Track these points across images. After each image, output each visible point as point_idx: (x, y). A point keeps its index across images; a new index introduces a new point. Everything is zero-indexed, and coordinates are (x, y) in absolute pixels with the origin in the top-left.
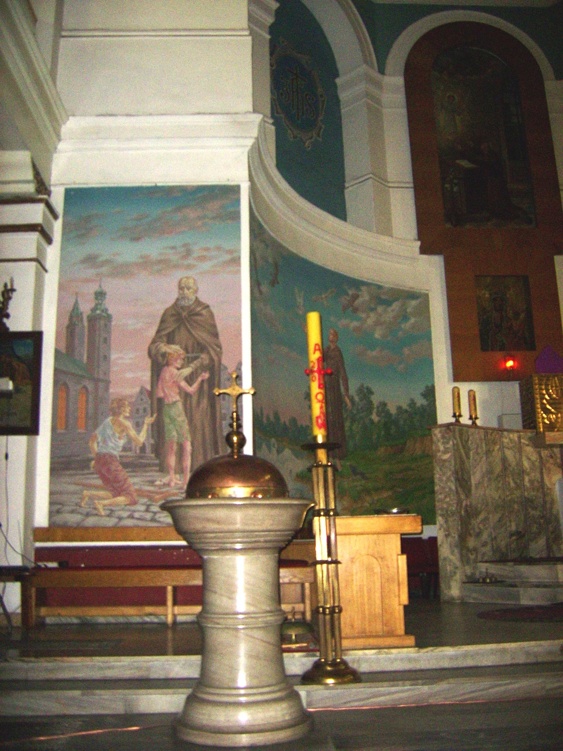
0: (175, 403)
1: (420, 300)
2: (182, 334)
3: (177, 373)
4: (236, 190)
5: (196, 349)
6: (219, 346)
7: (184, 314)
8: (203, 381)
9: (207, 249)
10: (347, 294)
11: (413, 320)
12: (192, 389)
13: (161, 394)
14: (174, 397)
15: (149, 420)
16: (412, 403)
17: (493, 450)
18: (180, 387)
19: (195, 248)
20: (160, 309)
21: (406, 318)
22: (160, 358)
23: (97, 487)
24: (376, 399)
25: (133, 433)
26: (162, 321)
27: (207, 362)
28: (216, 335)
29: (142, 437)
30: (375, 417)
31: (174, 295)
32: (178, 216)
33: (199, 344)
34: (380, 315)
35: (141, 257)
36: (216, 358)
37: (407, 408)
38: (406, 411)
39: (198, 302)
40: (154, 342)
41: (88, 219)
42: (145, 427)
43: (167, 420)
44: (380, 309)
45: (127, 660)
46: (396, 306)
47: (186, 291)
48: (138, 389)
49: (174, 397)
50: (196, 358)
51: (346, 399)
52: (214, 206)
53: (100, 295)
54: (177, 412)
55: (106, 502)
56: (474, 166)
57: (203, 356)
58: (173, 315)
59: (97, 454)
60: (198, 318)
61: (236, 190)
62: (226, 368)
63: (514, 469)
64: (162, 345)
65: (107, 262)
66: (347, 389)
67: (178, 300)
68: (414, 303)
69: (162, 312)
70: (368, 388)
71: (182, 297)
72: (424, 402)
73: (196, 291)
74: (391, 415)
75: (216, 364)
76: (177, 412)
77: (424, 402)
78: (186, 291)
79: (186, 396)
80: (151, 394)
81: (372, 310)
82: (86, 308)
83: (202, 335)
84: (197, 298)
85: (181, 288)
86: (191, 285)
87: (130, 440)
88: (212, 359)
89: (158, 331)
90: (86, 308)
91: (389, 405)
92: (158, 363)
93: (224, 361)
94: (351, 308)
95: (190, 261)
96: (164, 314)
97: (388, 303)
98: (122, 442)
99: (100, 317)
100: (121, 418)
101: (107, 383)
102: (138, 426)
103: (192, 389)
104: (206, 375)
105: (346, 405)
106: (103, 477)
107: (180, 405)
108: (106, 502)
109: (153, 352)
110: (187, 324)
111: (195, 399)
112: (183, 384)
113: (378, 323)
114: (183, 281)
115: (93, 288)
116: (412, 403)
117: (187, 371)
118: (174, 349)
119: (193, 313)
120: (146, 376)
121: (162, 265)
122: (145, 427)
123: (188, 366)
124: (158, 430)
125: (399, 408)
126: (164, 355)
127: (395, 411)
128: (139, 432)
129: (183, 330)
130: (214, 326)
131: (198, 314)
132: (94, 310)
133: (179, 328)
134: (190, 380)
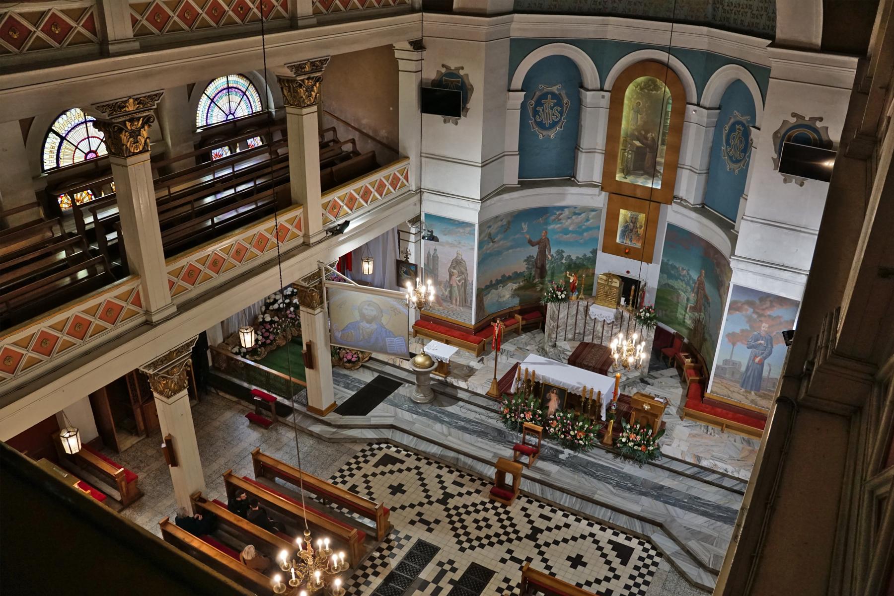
2: (457, 268)
3: (456, 279)
4: (473, 225)
5: (461, 273)
16: (585, 255)
21: (588, 220)
24: (565, 255)
29: (447, 293)
30: (564, 261)
44: (574, 217)
45: (253, 531)
46: (583, 215)
49: (455, 285)
52: (468, 229)
53: (435, 250)
54: (456, 289)
61: (473, 225)
68: (593, 213)
72: (591, 255)
76: (456, 289)
77: (591, 255)
82: (432, 253)
83: (463, 269)
90: (432, 253)
97: (580, 214)
110: (457, 263)
113: (571, 224)
116: (585, 255)
118: (455, 271)
120: (448, 277)
124: (451, 292)
125: (578, 258)
134: (459, 281)
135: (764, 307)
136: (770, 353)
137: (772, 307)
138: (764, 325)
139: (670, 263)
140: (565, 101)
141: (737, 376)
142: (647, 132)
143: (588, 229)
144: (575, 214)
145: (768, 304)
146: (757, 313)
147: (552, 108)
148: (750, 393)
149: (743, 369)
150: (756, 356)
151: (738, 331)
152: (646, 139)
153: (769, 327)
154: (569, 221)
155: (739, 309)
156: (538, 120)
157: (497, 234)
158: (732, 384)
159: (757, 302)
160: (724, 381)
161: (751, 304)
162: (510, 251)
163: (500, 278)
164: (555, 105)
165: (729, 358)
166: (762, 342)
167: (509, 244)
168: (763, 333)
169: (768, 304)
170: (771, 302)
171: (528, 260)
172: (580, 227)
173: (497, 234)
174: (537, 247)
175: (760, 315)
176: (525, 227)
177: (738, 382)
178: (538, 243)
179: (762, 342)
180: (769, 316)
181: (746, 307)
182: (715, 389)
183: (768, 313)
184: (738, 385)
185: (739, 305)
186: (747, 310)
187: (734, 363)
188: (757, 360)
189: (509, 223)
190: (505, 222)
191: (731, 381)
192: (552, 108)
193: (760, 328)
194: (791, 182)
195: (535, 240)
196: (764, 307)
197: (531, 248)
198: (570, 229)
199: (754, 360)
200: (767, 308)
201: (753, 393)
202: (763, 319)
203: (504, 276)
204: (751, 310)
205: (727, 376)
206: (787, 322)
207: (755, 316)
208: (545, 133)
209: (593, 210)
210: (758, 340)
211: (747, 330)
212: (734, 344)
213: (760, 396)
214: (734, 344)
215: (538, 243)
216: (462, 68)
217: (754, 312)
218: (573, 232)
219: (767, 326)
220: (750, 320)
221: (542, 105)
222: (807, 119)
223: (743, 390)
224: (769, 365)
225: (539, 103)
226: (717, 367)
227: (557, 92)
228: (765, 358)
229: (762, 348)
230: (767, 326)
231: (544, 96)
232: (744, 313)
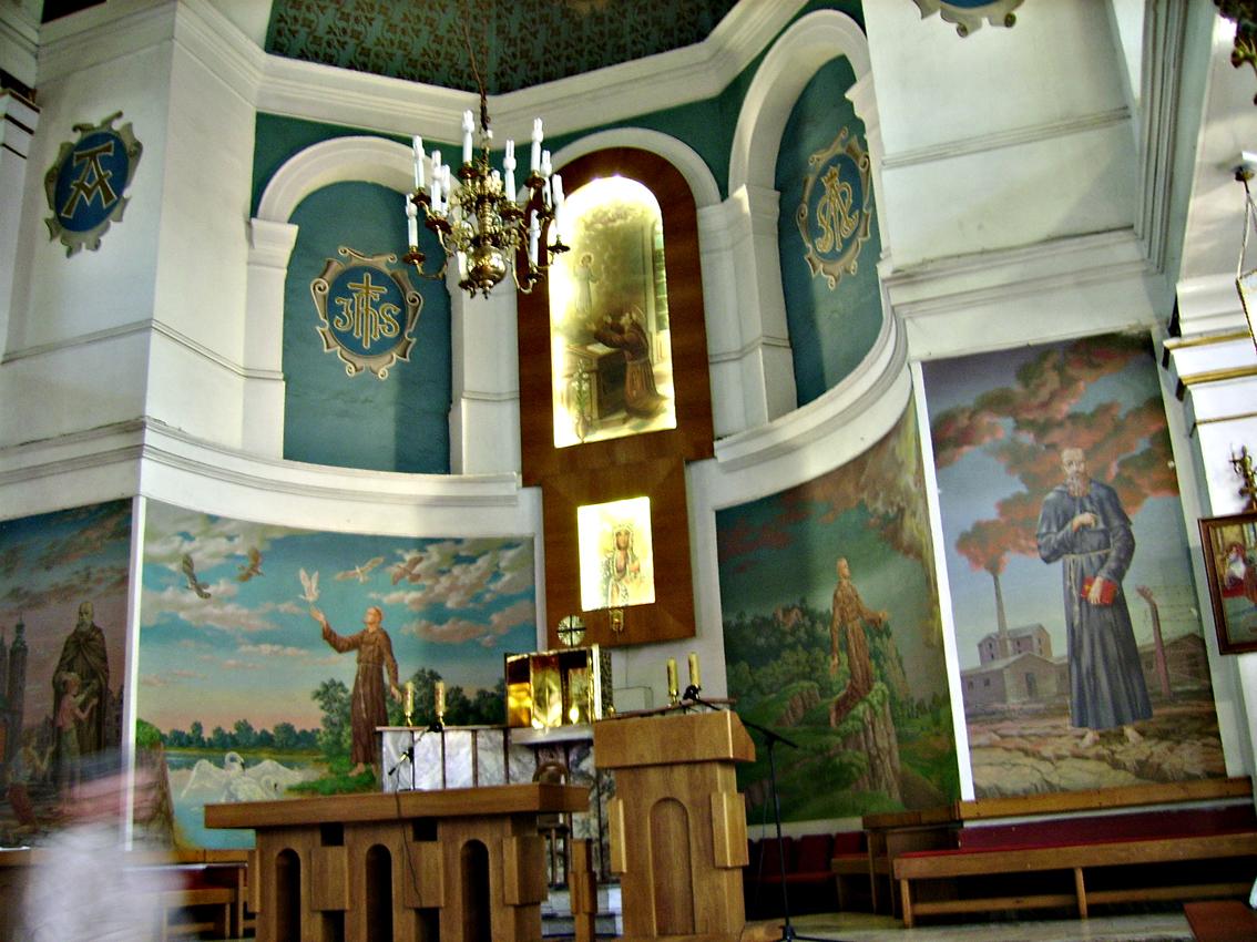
0: (70, 731)
1: (520, 548)
3: (73, 700)
6: (107, 671)
7: (82, 639)
8: (92, 709)
9: (103, 571)
10: (403, 560)
11: (507, 577)
12: (83, 716)
13: (61, 723)
14: (70, 725)
15: (50, 749)
17: (458, 753)
18: (74, 715)
19: (93, 570)
20: (62, 637)
21: (496, 575)
22: (62, 687)
23: (9, 817)
25: (38, 763)
26: (65, 649)
27: (96, 687)
28: (104, 659)
29: (44, 766)
31: (75, 622)
32: (83, 538)
33: (92, 670)
34: (457, 578)
35: (52, 586)
36: (104, 684)
37: (495, 691)
38: (493, 695)
39: (94, 627)
40: (57, 671)
41: (14, 552)
42: (48, 756)
43: (64, 749)
44: (457, 570)
46: (482, 562)
47: (85, 616)
48: (43, 718)
50: (88, 685)
51: (394, 690)
55: (16, 831)
56: (613, 350)
57: (94, 681)
58: (74, 642)
59: (12, 784)
60: (92, 643)
62: (111, 692)
63: (492, 775)
64: (63, 673)
65: (26, 594)
66: (395, 678)
67: (78, 626)
68: (511, 553)
69: (65, 640)
70: (431, 673)
71: (82, 623)
73: (92, 616)
74: (469, 702)
75: (104, 687)
78: (85, 616)
79: (79, 722)
80: (53, 723)
81: (443, 573)
83: (93, 660)
84: (93, 624)
85: (81, 614)
86: (90, 609)
87: (36, 769)
88: (101, 685)
89: (62, 660)
90: (1197, 725)
91: (464, 690)
92: (60, 691)
93: (111, 686)
94: (407, 577)
95: (90, 585)
96: (67, 642)
97: (471, 560)
98: (30, 771)
99: (19, 650)
100: (30, 749)
101: (21, 713)
102: (42, 755)
103: (83, 716)
104: (95, 701)
105: (393, 696)
106: (15, 807)
107: (74, 732)
108: (16, 831)
109: (57, 680)
111: (86, 725)
112: (78, 711)
113: (451, 589)
114: (83, 607)
115: (16, 620)
117: (81, 698)
118: (72, 677)
119: (89, 639)
120: (50, 703)
121: (65, 592)
122: (48, 756)
123: (82, 693)
126: (65, 683)
127: (476, 697)
128: (42, 761)
129: (80, 657)
130: (104, 650)
131: (93, 639)
132: (14, 643)
133: (77, 654)
134: (83, 707)
135: (1044, 394)
136: (1129, 549)
137: (1067, 383)
138: (1067, 454)
139: (748, 620)
140: (410, 294)
141: (1050, 686)
142: (617, 314)
143: (503, 601)
144: (458, 560)
145: (1052, 380)
146: (1031, 424)
147: (376, 306)
148: (1121, 737)
149: (1060, 649)
150: (1084, 581)
151: (989, 512)
152: (620, 330)
153: (1087, 455)
154: (445, 581)
155: (966, 437)
156: (341, 328)
157: (219, 572)
158: (1042, 726)
159: (1016, 387)
160: (1010, 728)
161: (999, 403)
162: (266, 648)
163: (230, 729)
164: (383, 299)
165: (991, 627)
166: (1086, 518)
167: (258, 624)
168: (1077, 487)
169: (1052, 380)
170: (1059, 369)
171: (327, 693)
172: (477, 598)
173: (219, 572)
174: (353, 655)
175: (1041, 429)
176: (310, 584)
177: (1062, 711)
178: (354, 644)
179: (1086, 518)
180: (1074, 417)
181: (986, 419)
182: (991, 777)
183: (1065, 407)
184: (1066, 723)
185: (963, 421)
186: (992, 429)
187: (1021, 641)
188: (1095, 592)
189: (256, 556)
190: (241, 548)
191: (1037, 715)
192: (376, 306)
193: (1057, 469)
194: (977, 26)
195: (346, 632)
196: (1044, 394)
197: (334, 655)
198: (450, 604)
199: (1084, 599)
200: (1053, 395)
201: (1129, 731)
202: (1055, 436)
203: (244, 727)
204: (1005, 425)
205: (1013, 702)
206: (1136, 413)
207: (1027, 438)
208: (360, 363)
209: (509, 544)
210: (1068, 517)
211: (1018, 498)
212: (994, 568)
213: (1162, 736)
214: (994, 568)
215: (354, 644)
216: (119, 115)
217: (1019, 426)
218: (461, 614)
219: (1077, 454)
220: (1016, 459)
221: (348, 294)
222: (985, 21)
223: (1090, 736)
224: (1144, 593)
225: (340, 287)
226: (968, 681)
227: (387, 271)
228: (1119, 574)
229: (1094, 540)
230: (1077, 454)
231: (354, 274)
232: (988, 440)
